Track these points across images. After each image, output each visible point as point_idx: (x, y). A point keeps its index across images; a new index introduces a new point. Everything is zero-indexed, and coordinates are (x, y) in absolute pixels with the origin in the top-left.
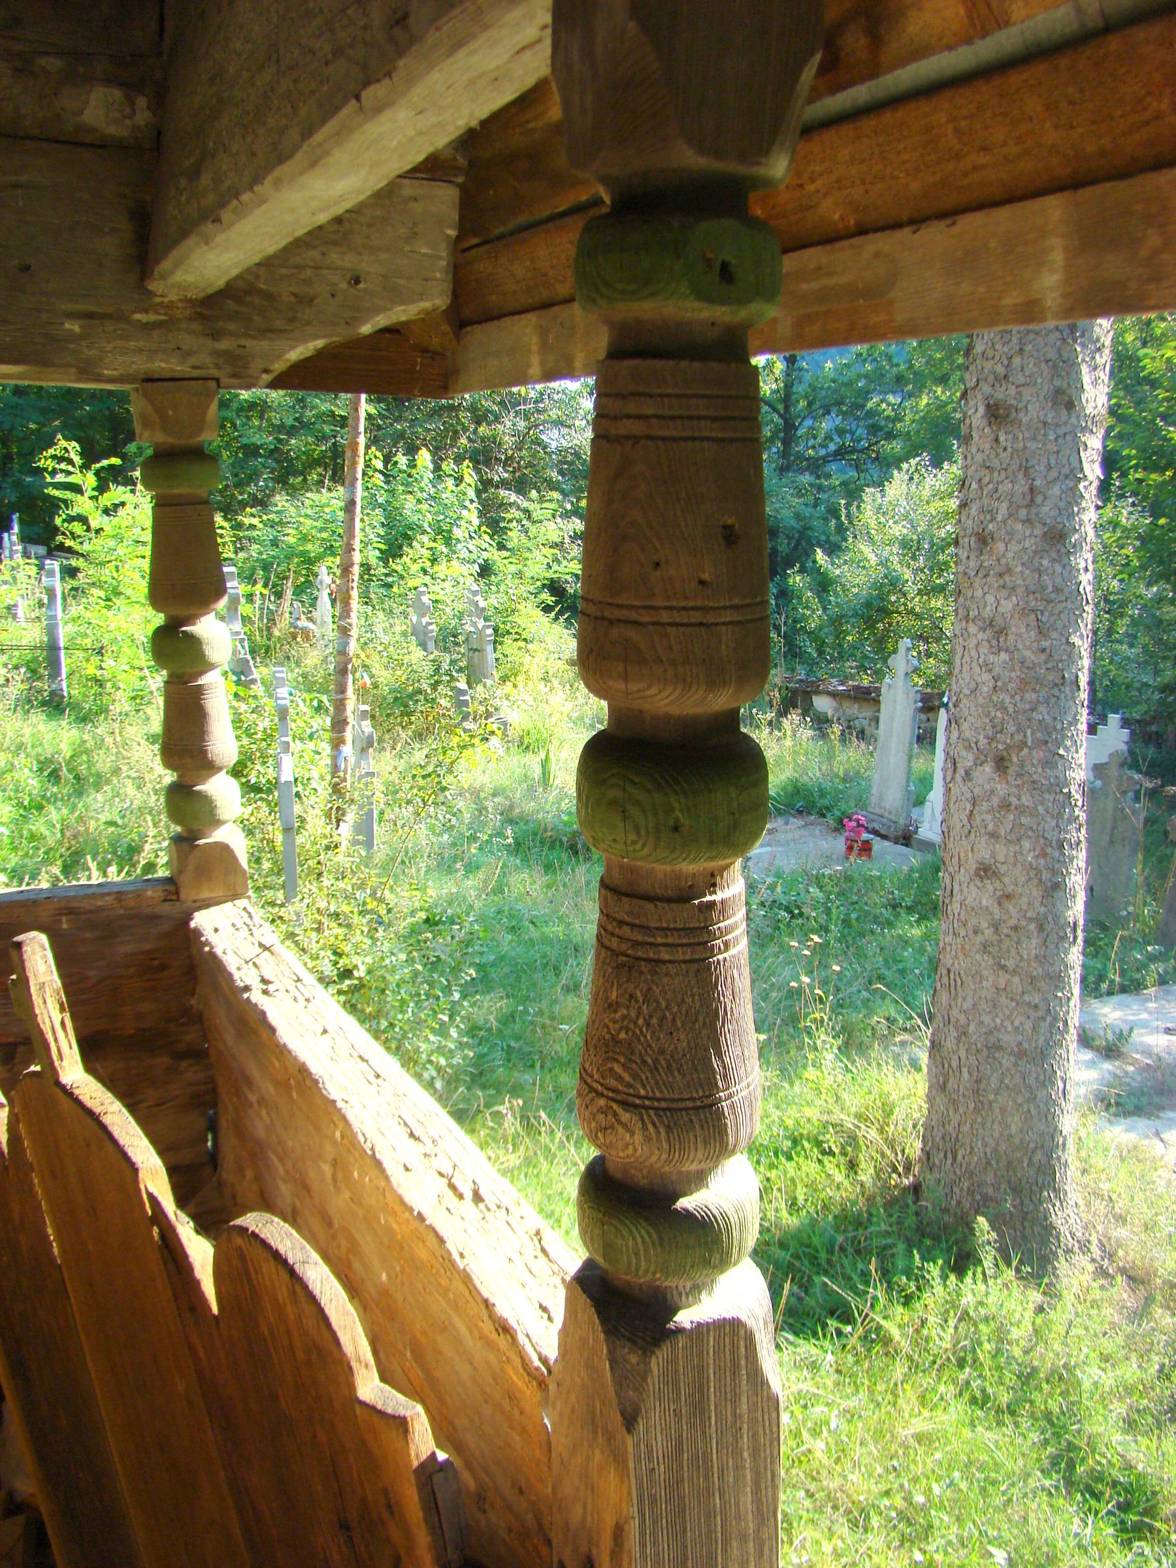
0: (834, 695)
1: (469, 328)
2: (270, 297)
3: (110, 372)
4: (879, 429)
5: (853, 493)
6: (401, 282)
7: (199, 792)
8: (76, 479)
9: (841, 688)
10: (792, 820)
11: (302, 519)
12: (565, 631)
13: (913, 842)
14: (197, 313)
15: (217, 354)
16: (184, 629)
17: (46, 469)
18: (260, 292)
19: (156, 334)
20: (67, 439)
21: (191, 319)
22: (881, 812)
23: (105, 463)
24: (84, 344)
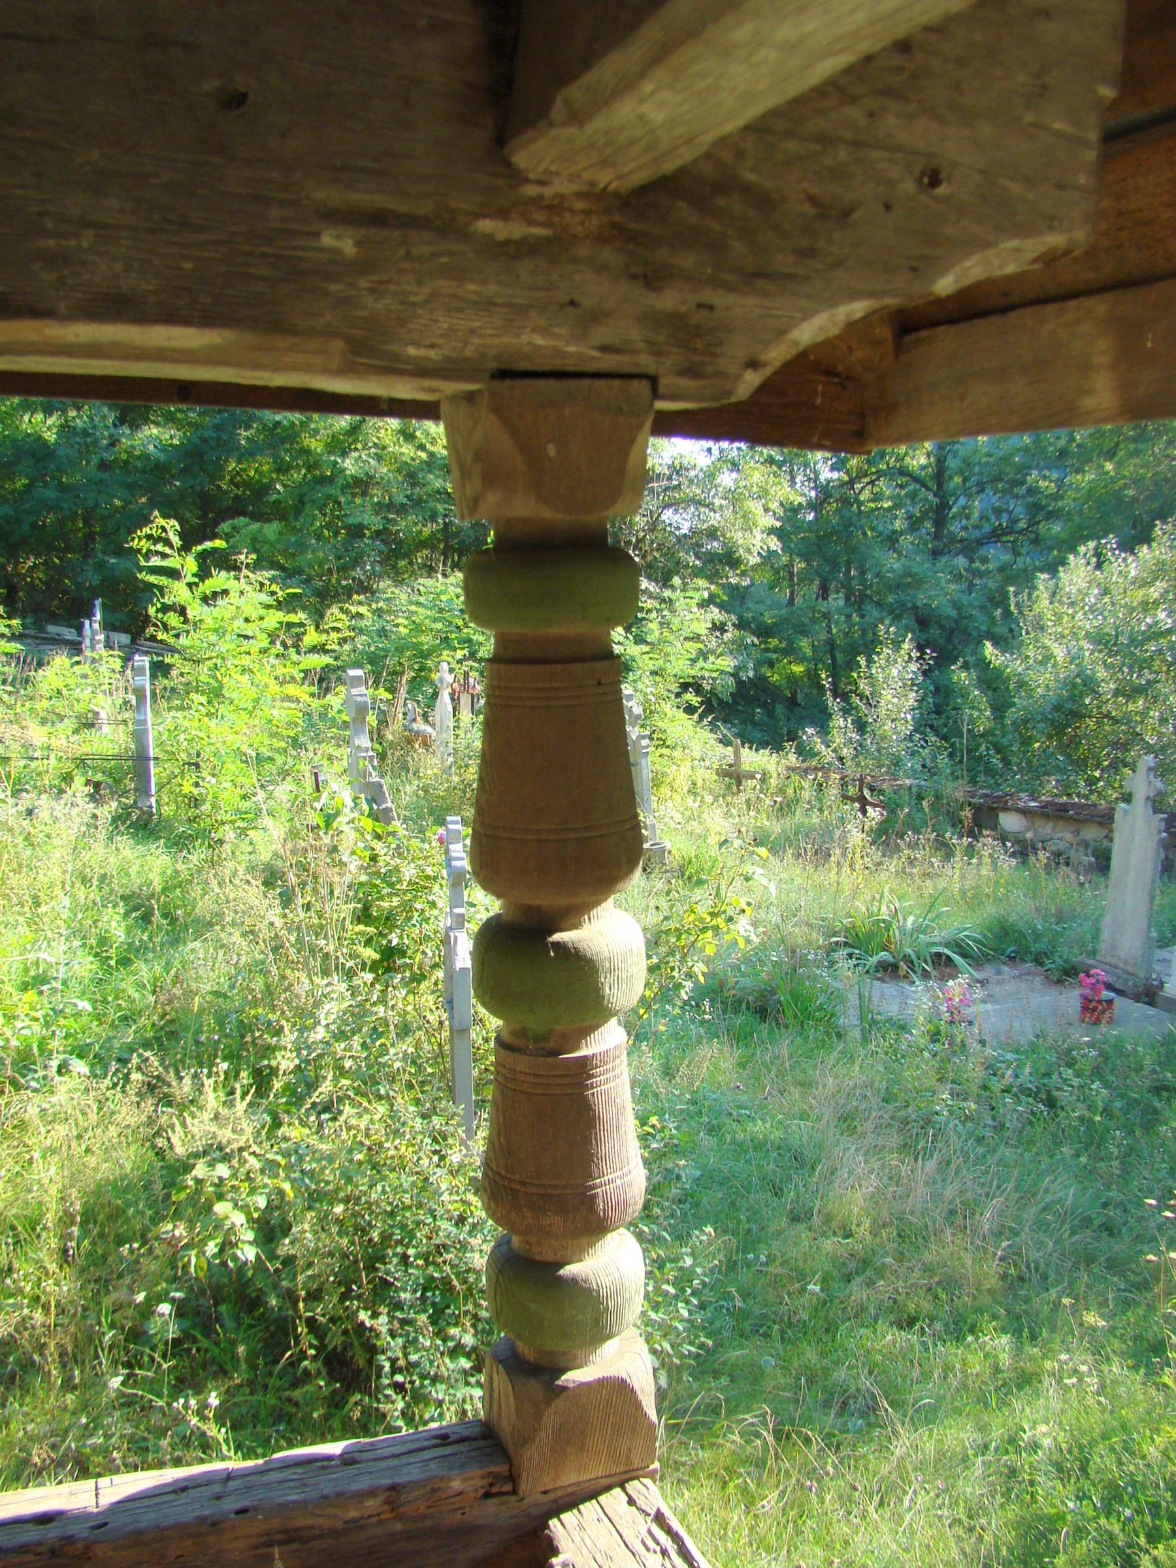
0: (1024, 812)
1: (923, 334)
2: (765, 202)
3: (422, 352)
4: (1039, 510)
5: (1025, 579)
6: (1015, 188)
7: (573, 1283)
8: (173, 563)
9: (1033, 804)
10: (1005, 969)
11: (413, 608)
12: (711, 735)
13: (1158, 1000)
14: (614, 225)
15: (652, 319)
16: (557, 937)
17: (139, 551)
18: (746, 189)
19: (524, 269)
20: (165, 516)
21: (601, 239)
22: (1114, 961)
23: (208, 545)
24: (363, 283)
